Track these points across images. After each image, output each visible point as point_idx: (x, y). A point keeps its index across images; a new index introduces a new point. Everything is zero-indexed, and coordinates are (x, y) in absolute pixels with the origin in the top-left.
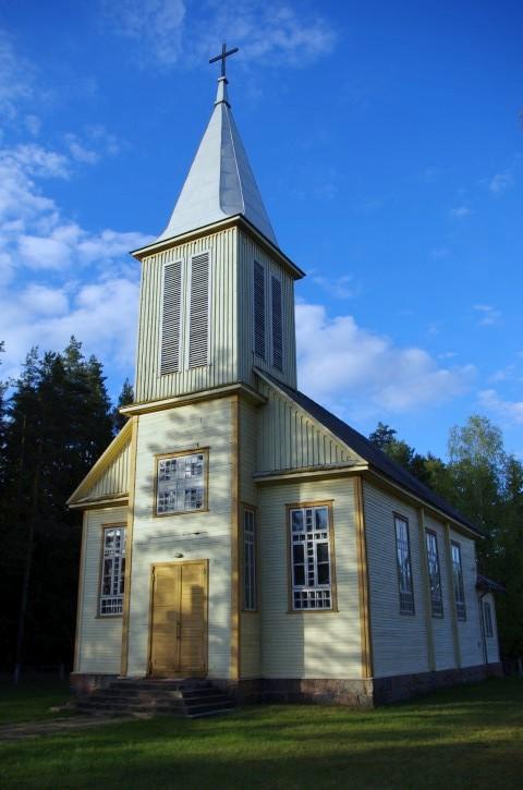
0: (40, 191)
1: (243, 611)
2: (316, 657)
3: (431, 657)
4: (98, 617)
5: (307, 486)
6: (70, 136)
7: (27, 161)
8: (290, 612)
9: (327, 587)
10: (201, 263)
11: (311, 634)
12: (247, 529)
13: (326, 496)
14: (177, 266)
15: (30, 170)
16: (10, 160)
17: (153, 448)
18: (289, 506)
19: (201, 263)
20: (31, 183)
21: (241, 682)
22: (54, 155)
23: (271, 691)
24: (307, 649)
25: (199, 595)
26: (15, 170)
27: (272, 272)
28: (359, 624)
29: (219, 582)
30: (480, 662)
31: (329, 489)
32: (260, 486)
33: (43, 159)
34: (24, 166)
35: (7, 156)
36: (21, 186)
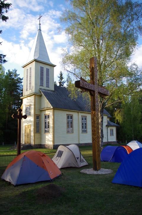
0: (56, 22)
1: (36, 133)
2: (47, 141)
3: (79, 140)
4: (67, 133)
5: (47, 111)
6: (61, 5)
7: (52, 15)
8: (44, 133)
9: (49, 129)
10: (30, 68)
11: (47, 137)
12: (37, 119)
13: (49, 113)
14: (28, 69)
15: (53, 17)
16: (47, 15)
17: (25, 105)
18: (45, 115)
19: (30, 68)
20: (54, 20)
21: (34, 145)
22: (58, 12)
23: (41, 146)
24: (46, 140)
25: (30, 131)
26: (49, 18)
27: (45, 67)
28: (52, 135)
29: (32, 128)
30: (107, 141)
31: (49, 111)
32: (41, 111)
33: (55, 13)
34: (51, 16)
35: (46, 14)
36: (51, 22)
